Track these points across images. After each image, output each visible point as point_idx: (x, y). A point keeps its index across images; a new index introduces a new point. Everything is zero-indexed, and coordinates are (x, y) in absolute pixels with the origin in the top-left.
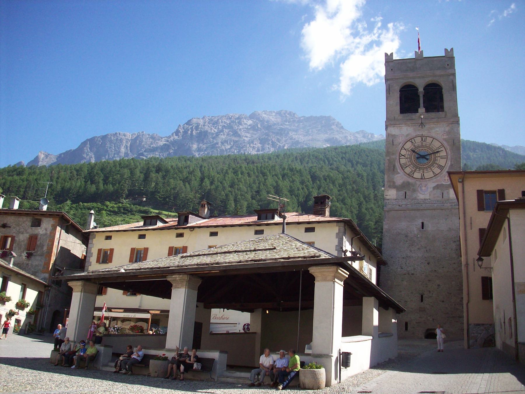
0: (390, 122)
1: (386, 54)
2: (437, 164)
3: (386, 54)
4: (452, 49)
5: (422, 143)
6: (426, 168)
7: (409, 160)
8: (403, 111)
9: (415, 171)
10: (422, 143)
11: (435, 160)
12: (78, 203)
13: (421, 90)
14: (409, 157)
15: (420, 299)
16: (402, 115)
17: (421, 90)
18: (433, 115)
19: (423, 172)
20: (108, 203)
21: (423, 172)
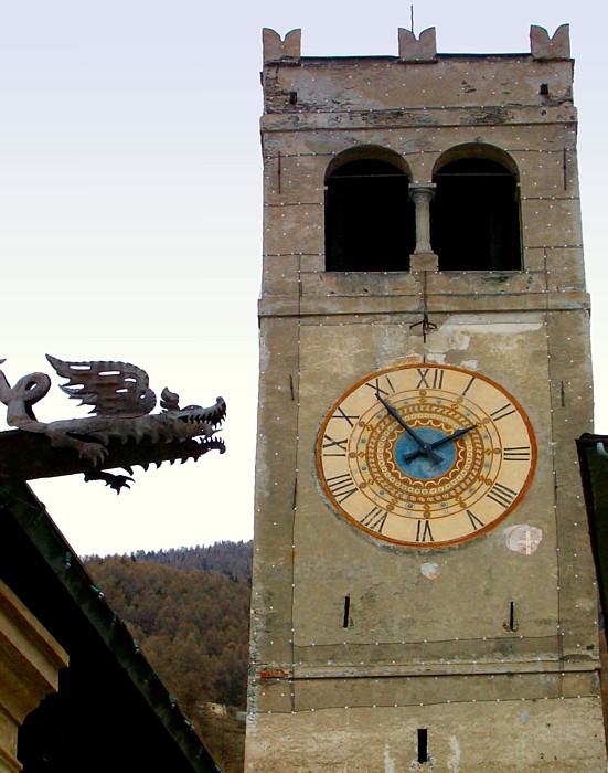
0: (282, 318)
1: (269, 35)
2: (487, 481)
3: (269, 35)
4: (563, 31)
5: (423, 393)
6: (441, 499)
7: (363, 462)
8: (339, 259)
9: (390, 508)
10: (423, 393)
11: (479, 464)
12: (202, 443)
13: (422, 178)
14: (363, 448)
15: (342, 623)
16: (335, 277)
17: (422, 178)
18: (470, 282)
19: (427, 515)
20: (199, 442)
21: (427, 515)
